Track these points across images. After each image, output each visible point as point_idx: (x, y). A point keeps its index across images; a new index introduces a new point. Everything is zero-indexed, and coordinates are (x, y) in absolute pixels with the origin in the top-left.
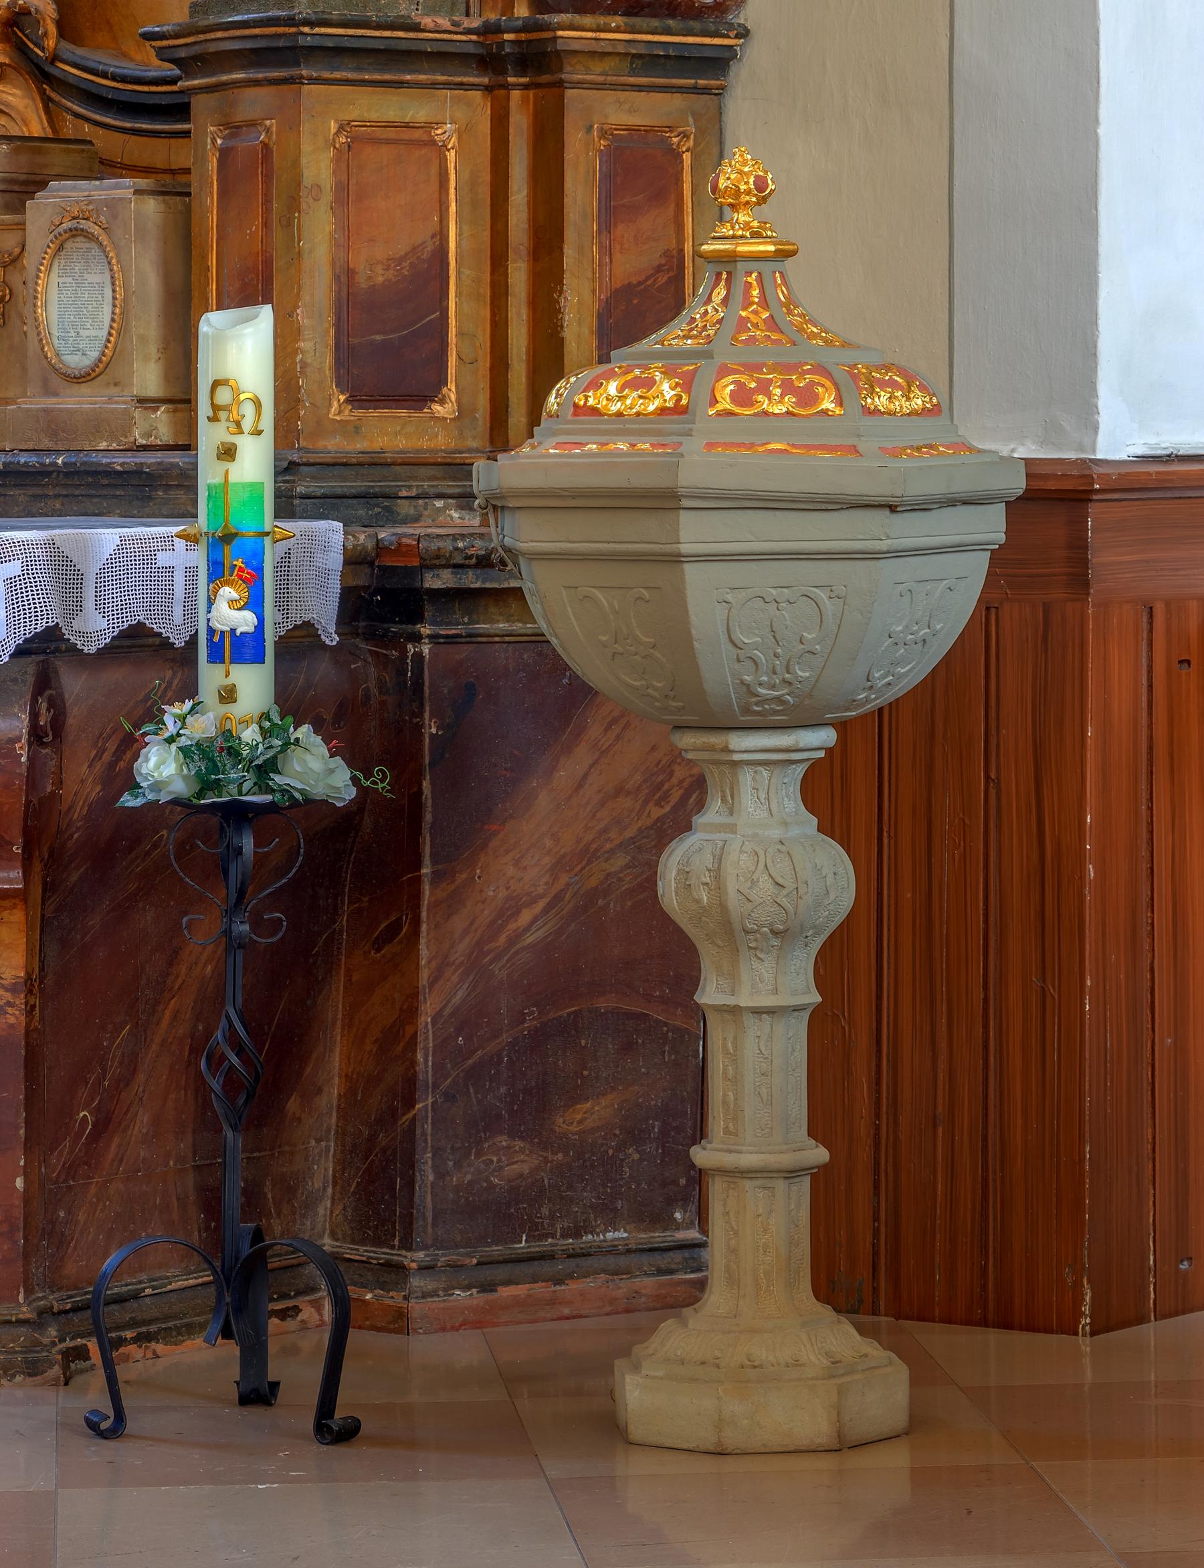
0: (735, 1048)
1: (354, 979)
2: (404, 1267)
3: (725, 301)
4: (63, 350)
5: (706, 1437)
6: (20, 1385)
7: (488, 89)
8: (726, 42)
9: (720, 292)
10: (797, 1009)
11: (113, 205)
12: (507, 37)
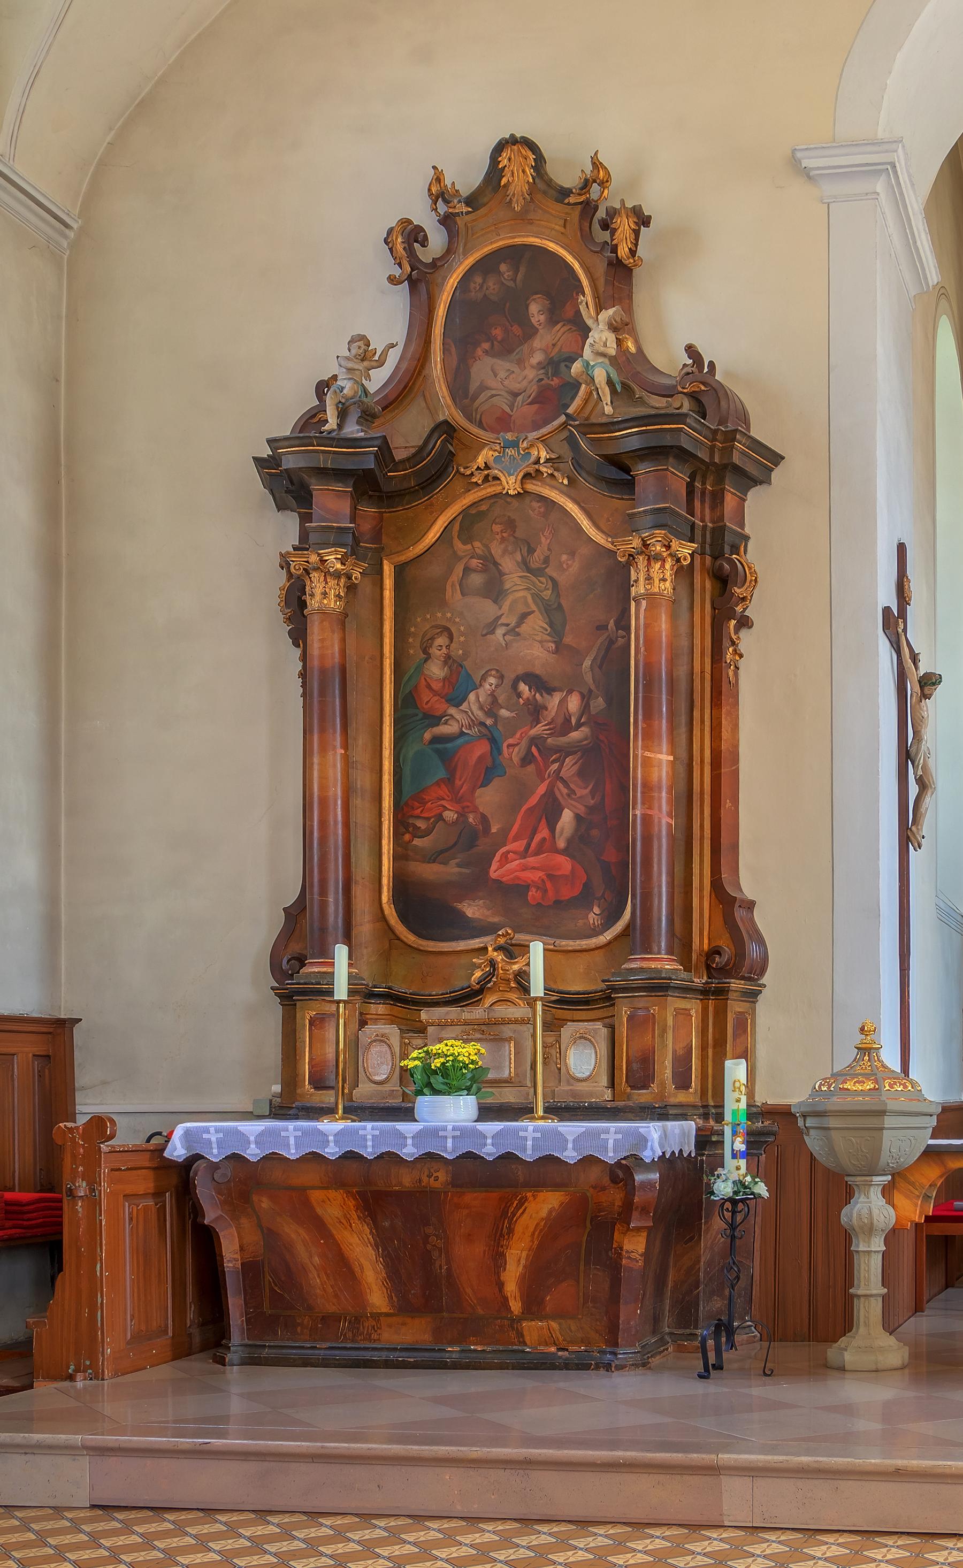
0: (868, 1262)
1: (677, 1253)
2: (696, 1335)
3: (869, 1060)
4: (575, 1072)
5: (874, 1368)
6: (641, 1370)
7: (701, 1000)
8: (760, 988)
9: (866, 1058)
10: (878, 1252)
11: (595, 1030)
12: (714, 985)
